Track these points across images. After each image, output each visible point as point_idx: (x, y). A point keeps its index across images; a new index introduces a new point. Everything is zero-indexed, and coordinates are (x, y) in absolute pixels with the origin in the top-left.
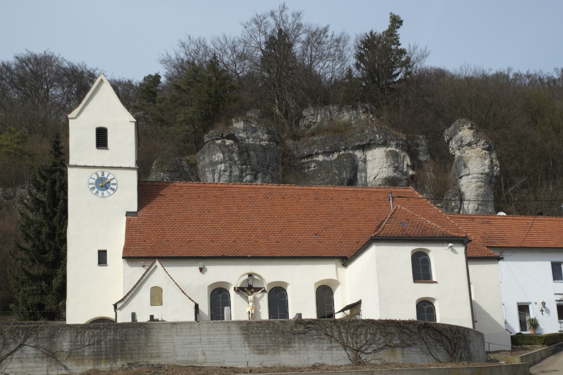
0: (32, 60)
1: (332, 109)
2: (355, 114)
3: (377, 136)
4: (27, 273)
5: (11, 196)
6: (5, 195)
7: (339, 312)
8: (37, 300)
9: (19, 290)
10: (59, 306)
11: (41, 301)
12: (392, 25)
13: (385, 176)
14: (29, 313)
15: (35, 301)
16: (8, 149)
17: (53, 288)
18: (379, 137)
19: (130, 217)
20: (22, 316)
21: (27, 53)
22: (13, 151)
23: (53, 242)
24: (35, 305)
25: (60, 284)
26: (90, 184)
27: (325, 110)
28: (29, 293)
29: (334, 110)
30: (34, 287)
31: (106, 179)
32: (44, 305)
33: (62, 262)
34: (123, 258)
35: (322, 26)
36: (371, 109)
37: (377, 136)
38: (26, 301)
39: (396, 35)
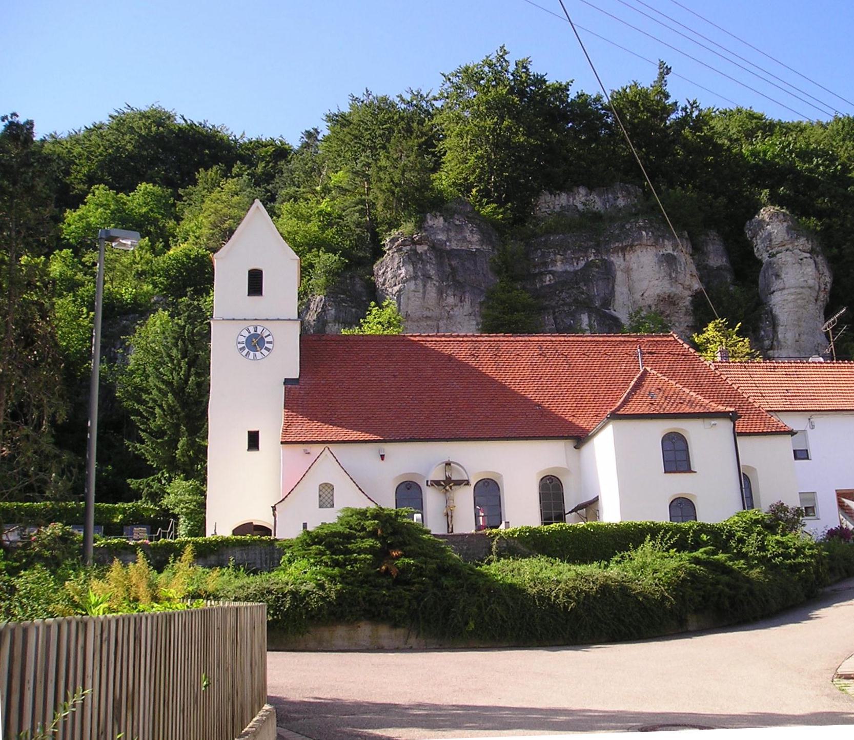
3: (644, 233)
7: (570, 513)
13: (658, 291)
18: (647, 234)
19: (289, 386)
37: (644, 233)
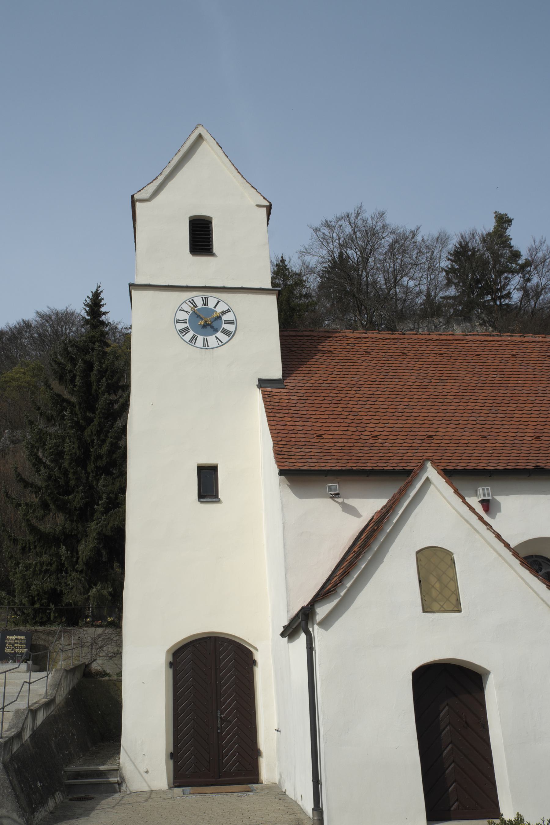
0: (53, 317)
1: (437, 322)
2: (469, 327)
4: (33, 529)
5: (19, 440)
6: (12, 438)
8: (49, 584)
9: (17, 564)
10: (89, 596)
11: (57, 584)
12: (498, 226)
14: (34, 609)
15: (45, 586)
16: (20, 383)
17: (80, 560)
20: (19, 615)
21: (49, 309)
22: (26, 385)
23: (83, 472)
24: (45, 593)
25: (91, 551)
26: (178, 322)
27: (429, 322)
28: (35, 570)
29: (440, 322)
30: (45, 558)
31: (212, 311)
32: (61, 593)
33: (96, 507)
34: (282, 473)
35: (412, 227)
36: (490, 321)
38: (29, 586)
39: (505, 236)
